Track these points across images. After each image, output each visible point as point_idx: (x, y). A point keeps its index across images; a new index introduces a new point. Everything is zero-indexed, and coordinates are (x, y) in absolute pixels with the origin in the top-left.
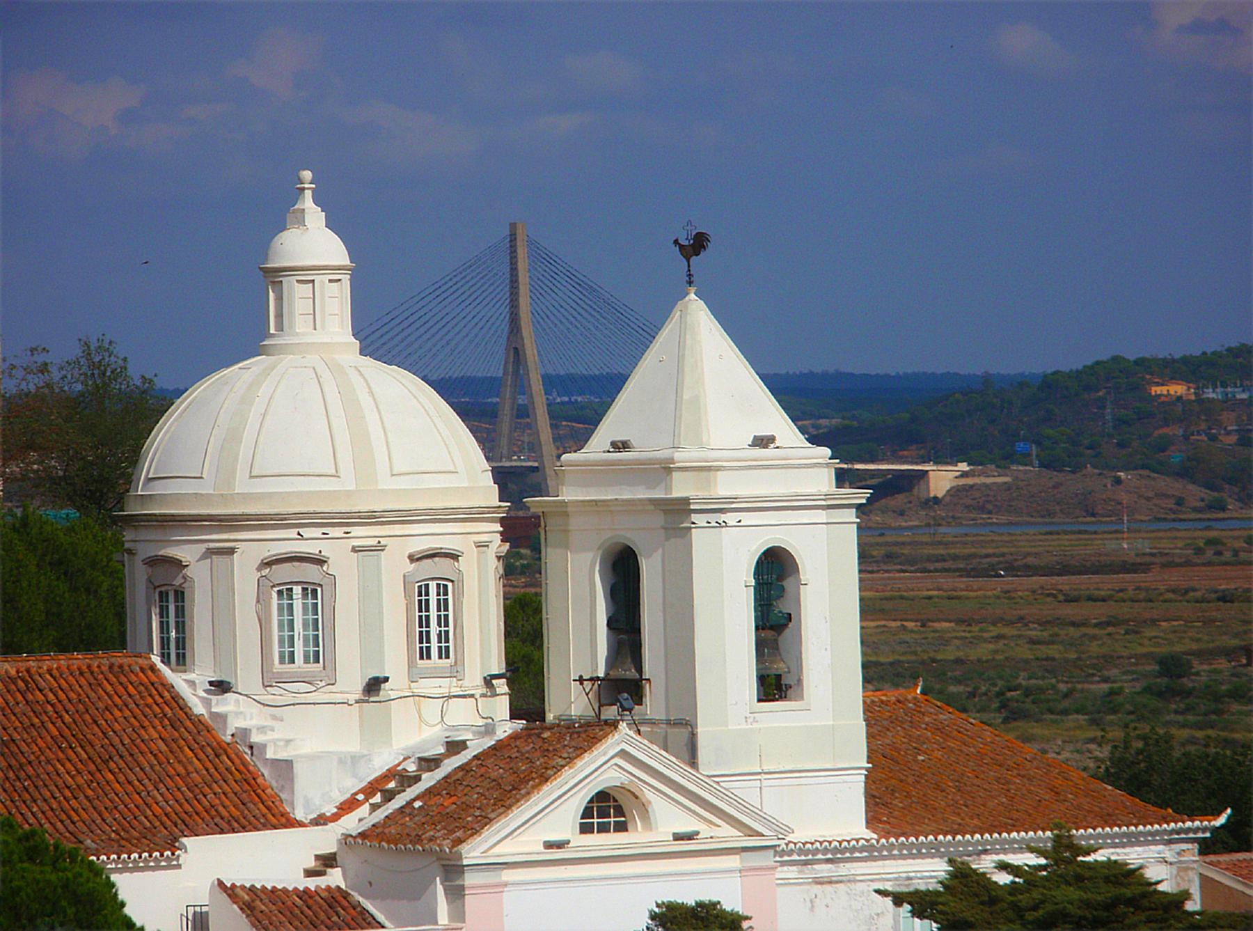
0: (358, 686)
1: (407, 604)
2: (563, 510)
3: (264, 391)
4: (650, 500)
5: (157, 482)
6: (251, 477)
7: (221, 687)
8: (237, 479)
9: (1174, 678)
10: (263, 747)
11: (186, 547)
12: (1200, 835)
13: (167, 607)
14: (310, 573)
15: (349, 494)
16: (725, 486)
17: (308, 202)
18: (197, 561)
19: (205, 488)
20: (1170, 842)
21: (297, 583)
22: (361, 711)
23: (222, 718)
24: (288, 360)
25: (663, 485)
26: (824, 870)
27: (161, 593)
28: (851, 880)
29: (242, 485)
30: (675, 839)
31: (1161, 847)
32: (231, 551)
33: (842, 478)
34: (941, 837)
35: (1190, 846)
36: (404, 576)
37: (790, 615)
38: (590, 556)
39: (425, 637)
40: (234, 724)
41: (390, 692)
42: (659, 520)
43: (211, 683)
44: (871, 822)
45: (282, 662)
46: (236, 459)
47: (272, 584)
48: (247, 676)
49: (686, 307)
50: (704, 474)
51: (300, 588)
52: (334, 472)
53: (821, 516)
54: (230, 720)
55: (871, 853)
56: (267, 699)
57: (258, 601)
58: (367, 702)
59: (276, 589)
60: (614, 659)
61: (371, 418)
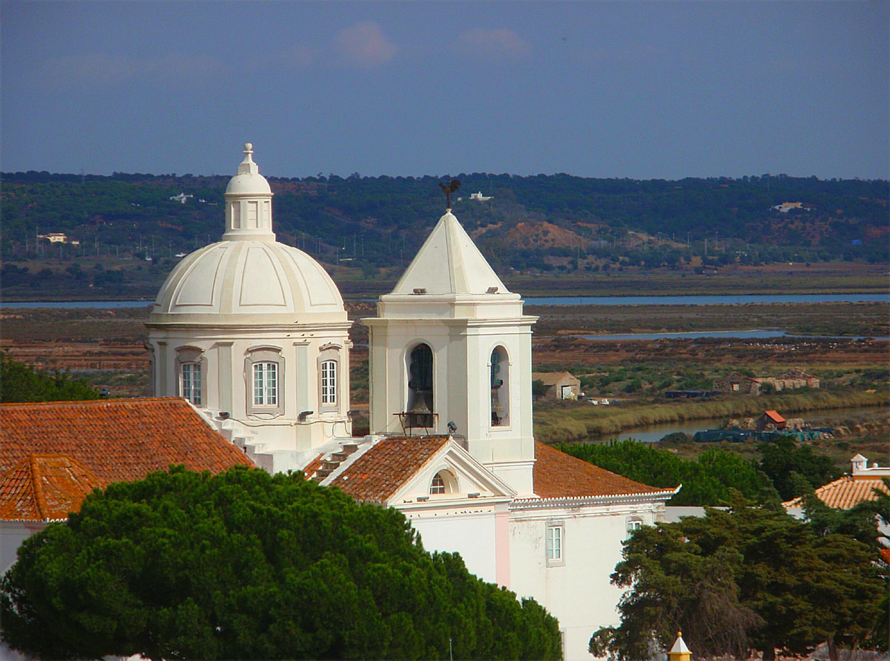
0: (296, 416)
2: (385, 324)
3: (241, 259)
4: (443, 321)
5: (182, 307)
6: (240, 305)
7: (225, 416)
9: (677, 418)
10: (253, 448)
11: (203, 342)
12: (667, 498)
13: (189, 373)
14: (272, 356)
15: (292, 315)
16: (481, 314)
17: (250, 160)
18: (211, 349)
19: (215, 311)
20: (655, 502)
21: (265, 362)
22: (297, 427)
23: (229, 432)
24: (246, 244)
25: (449, 312)
26: (519, 514)
27: (185, 366)
28: (529, 520)
29: (236, 310)
30: (469, 497)
31: (650, 504)
32: (232, 344)
33: (527, 310)
34: (568, 498)
35: (661, 504)
37: (502, 381)
38: (400, 351)
39: (325, 391)
40: (236, 435)
42: (446, 330)
43: (221, 414)
44: (535, 490)
45: (256, 403)
46: (231, 296)
48: (238, 410)
49: (448, 219)
50: (470, 307)
52: (283, 304)
53: (517, 330)
54: (233, 433)
55: (539, 506)
59: (182, 365)
60: (414, 401)
61: (298, 275)
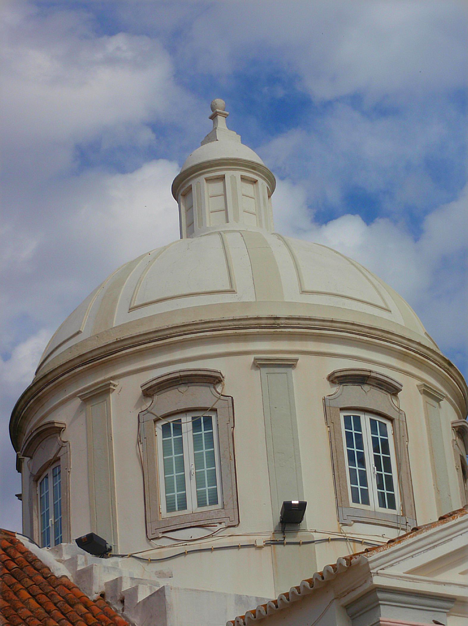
1: (330, 432)
8: (115, 319)
36: (324, 399)
41: (314, 534)
45: (170, 508)
47: (155, 418)
51: (189, 419)
52: (228, 288)
56: (153, 554)
57: (139, 441)
58: (282, 543)
59: (159, 425)
